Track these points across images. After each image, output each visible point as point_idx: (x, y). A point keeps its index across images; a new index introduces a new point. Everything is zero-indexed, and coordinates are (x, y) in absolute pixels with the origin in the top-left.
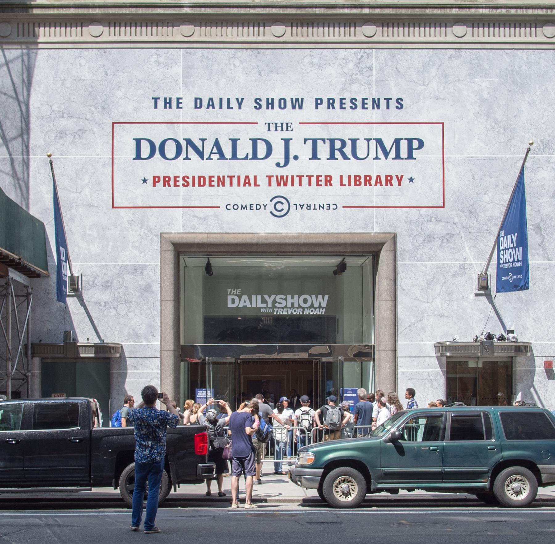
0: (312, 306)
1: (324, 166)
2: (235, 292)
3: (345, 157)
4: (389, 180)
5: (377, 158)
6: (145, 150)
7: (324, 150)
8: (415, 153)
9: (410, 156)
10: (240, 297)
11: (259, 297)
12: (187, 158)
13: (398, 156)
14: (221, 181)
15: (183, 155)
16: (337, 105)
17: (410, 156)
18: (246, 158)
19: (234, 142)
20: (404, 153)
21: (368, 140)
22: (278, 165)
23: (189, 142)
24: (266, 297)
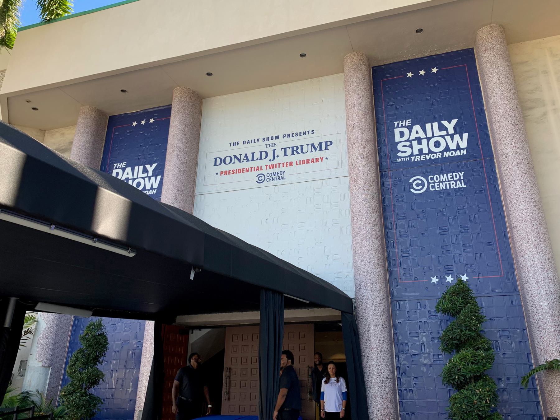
0: (447, 149)
1: (290, 158)
2: (404, 123)
3: (298, 153)
4: (317, 160)
5: (312, 151)
6: (218, 161)
7: (289, 152)
8: (328, 147)
9: (326, 149)
10: (410, 129)
11: (435, 125)
12: (234, 163)
13: (321, 149)
14: (247, 170)
15: (233, 162)
16: (291, 136)
17: (326, 149)
18: (257, 159)
19: (253, 154)
20: (323, 148)
21: (308, 145)
22: (270, 160)
23: (235, 156)
24: (445, 123)
